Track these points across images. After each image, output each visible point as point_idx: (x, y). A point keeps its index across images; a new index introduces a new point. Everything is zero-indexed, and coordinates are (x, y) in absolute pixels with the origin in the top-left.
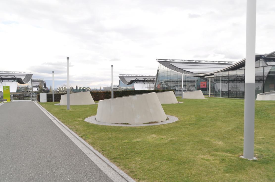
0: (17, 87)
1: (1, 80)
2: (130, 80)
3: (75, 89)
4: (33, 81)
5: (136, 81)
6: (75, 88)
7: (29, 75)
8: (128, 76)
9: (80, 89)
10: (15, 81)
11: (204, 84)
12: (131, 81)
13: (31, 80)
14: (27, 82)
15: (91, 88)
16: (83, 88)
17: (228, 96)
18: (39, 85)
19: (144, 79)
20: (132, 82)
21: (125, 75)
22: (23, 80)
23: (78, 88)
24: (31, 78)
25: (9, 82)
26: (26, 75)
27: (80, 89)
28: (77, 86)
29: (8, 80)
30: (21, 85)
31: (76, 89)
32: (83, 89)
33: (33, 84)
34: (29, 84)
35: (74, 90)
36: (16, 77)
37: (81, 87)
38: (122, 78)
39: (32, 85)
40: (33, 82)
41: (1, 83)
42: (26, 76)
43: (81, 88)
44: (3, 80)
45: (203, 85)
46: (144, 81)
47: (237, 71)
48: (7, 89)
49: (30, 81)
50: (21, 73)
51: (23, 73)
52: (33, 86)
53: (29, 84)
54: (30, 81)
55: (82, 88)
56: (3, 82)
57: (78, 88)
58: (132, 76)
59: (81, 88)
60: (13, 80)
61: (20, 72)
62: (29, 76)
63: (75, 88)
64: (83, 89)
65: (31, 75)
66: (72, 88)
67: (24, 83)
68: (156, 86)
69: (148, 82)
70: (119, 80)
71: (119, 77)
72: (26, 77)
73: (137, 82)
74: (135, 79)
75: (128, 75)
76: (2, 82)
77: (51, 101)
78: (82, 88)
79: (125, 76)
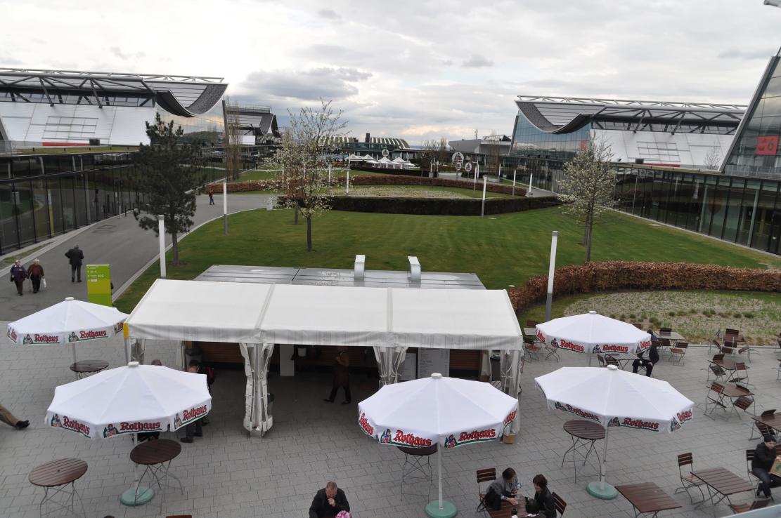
1: (100, 98)
2: (576, 115)
3: (362, 143)
6: (362, 139)
8: (548, 101)
9: (377, 142)
10: (150, 102)
12: (580, 116)
13: (219, 102)
15: (410, 143)
16: (387, 140)
17: (11, 100)
19: (632, 114)
20: (580, 123)
21: (537, 97)
23: (373, 141)
24: (221, 95)
26: (205, 87)
27: (377, 142)
28: (368, 135)
29: (124, 99)
30: (167, 117)
31: (365, 144)
32: (386, 142)
35: (360, 147)
36: (151, 88)
37: (380, 137)
38: (529, 109)
40: (227, 115)
42: (205, 90)
43: (379, 140)
47: (472, 138)
50: (190, 81)
51: (198, 81)
55: (383, 140)
56: (108, 104)
57: (373, 141)
58: (565, 101)
59: (379, 140)
60: (141, 100)
61: (189, 78)
62: (213, 91)
63: (362, 139)
64: (386, 142)
65: (223, 87)
66: (355, 139)
68: (144, 100)
69: (648, 126)
70: (517, 117)
71: (519, 104)
73: (603, 124)
74: (595, 112)
75: (548, 98)
78: (383, 140)
79: (540, 100)
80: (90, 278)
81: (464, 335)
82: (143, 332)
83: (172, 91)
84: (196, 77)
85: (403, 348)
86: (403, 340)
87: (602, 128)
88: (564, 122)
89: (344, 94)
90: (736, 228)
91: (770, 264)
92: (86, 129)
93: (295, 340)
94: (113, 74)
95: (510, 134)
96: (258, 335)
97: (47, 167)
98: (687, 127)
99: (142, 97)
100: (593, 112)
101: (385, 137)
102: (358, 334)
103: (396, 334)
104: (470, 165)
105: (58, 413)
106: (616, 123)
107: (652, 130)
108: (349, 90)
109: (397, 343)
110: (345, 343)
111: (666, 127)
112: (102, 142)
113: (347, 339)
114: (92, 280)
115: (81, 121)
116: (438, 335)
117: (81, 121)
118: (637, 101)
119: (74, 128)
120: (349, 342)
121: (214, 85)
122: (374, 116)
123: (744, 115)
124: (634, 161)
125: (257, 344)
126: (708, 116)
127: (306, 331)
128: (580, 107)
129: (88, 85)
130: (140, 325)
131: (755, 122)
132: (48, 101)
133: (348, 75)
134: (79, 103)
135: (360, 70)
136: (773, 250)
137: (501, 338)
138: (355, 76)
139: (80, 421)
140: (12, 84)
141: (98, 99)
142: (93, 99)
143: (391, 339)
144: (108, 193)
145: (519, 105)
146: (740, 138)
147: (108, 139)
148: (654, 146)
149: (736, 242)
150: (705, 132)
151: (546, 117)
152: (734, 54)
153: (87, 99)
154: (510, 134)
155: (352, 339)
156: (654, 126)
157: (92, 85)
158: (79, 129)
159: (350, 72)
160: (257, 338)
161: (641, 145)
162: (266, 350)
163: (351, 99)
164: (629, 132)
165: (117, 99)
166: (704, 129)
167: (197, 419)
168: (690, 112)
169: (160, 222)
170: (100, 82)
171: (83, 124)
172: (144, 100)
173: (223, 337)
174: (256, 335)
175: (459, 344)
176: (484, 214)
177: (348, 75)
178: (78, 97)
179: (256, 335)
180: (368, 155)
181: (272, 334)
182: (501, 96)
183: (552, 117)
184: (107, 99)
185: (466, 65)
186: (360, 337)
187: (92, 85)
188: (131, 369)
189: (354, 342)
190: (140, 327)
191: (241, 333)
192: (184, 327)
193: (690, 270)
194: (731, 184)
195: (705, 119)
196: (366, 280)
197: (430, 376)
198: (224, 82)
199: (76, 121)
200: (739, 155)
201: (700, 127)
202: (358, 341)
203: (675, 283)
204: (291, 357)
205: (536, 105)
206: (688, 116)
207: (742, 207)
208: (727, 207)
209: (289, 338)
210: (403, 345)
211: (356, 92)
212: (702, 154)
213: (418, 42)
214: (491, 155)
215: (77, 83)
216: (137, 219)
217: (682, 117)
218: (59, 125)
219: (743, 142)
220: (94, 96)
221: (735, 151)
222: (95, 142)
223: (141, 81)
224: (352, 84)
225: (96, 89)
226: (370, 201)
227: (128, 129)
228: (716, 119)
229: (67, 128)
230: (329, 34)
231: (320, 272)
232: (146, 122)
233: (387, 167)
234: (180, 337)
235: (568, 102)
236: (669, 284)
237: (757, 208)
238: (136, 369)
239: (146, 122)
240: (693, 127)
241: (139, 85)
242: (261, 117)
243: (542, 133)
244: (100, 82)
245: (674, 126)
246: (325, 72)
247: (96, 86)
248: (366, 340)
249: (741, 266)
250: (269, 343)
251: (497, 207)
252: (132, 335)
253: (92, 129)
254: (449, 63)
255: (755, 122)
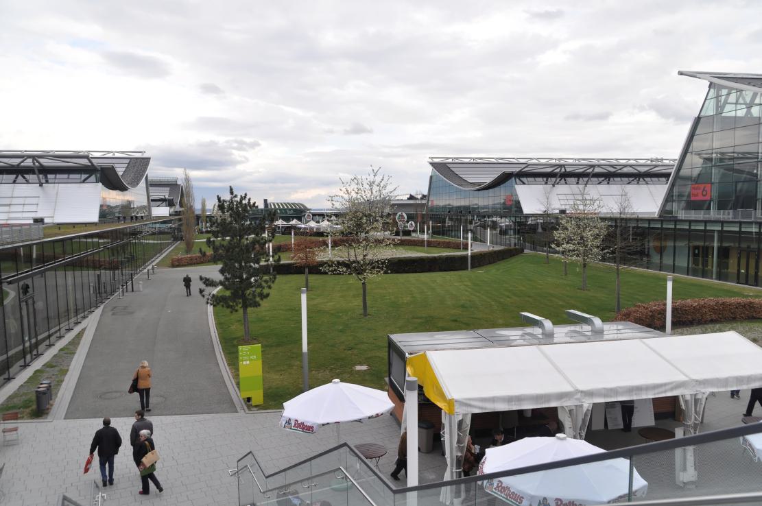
0: (101, 206)
1: (41, 176)
4: (152, 184)
5: (526, 174)
7: (139, 161)
8: (457, 161)
10: (93, 178)
11: (704, 190)
14: (135, 183)
18: (167, 197)
22: (120, 174)
25: (70, 181)
26: (128, 161)
30: (115, 198)
33: (151, 194)
34: (136, 196)
39: (148, 196)
40: (150, 188)
41: (41, 185)
44: (50, 176)
45: (701, 191)
46: (547, 176)
48: (251, 357)
49: (142, 184)
50: (110, 155)
51: (117, 155)
52: (153, 200)
53: (136, 196)
54: (142, 184)
56: (47, 182)
58: (472, 161)
60: (84, 176)
61: (109, 152)
62: (139, 164)
67: (122, 188)
68: (88, 175)
69: (563, 180)
70: (431, 177)
71: (432, 164)
72: (127, 167)
73: (524, 180)
74: (518, 170)
76: (44, 181)
77: (464, 269)
79: (450, 161)
80: (243, 361)
81: (752, 375)
82: (470, 406)
83: (116, 166)
84: (116, 152)
85: (704, 393)
86: (702, 386)
87: (524, 183)
88: (488, 180)
89: (233, 163)
90: (686, 265)
91: (751, 293)
92: (27, 208)
93: (611, 397)
94: (25, 151)
95: (426, 193)
96: (578, 396)
97: (35, 246)
98: (596, 179)
99: (84, 174)
100: (516, 169)
101: (275, 202)
102: (665, 385)
103: (697, 381)
104: (413, 223)
105: (546, 496)
106: (623, 179)
107: (566, 183)
108: (239, 159)
109: (699, 389)
110: (655, 394)
111: (578, 180)
112: (46, 221)
113: (656, 391)
114: (244, 363)
115: (21, 201)
116: (730, 377)
117: (21, 201)
118: (633, 160)
119: (13, 208)
120: (658, 393)
121: (137, 158)
122: (265, 182)
123: (675, 167)
124: (558, 211)
125: (576, 406)
126: (643, 169)
127: (620, 387)
128: (487, 166)
129: (29, 162)
130: (470, 399)
131: (683, 172)
132: (38, 181)
133: (235, 145)
134: (14, 182)
135: (248, 140)
136: (744, 282)
137: (671, 383)
138: (242, 146)
139: (577, 500)
140: (645, 172)
141: (38, 177)
142: (30, 177)
143: (694, 386)
144: (98, 272)
145: (433, 166)
146: (673, 186)
147: (52, 217)
148: (571, 197)
149: (688, 275)
150: (610, 183)
151: (457, 173)
152: (576, 117)
153: (24, 178)
154: (426, 193)
155: (660, 390)
156: (569, 180)
157: (34, 163)
158: (20, 208)
159: (236, 141)
160: (576, 399)
161: (561, 197)
162: (460, 423)
163: (240, 168)
164: (547, 186)
165: (58, 176)
166: (609, 180)
167: (506, 501)
168: (599, 166)
169: (668, 282)
170: (42, 161)
171: (14, 199)
172: (88, 175)
173: (545, 402)
174: (576, 397)
175: (747, 384)
176: (472, 267)
177: (235, 145)
178: (15, 176)
179: (576, 397)
180: (295, 220)
181: (590, 394)
182: (381, 158)
183: (468, 176)
184: (46, 177)
185: (347, 132)
186: (667, 387)
187: (34, 163)
188: (559, 441)
189: (662, 392)
190: (464, 401)
191: (561, 396)
192: (509, 396)
193: (723, 304)
194: (690, 227)
195: (609, 171)
196: (555, 336)
197: (554, 436)
198: (145, 155)
199: (15, 201)
200: (673, 201)
201: (606, 179)
202: (665, 391)
203: (713, 316)
204: (635, 410)
205: (449, 166)
206: (597, 170)
207: (689, 247)
208: (675, 247)
209: (605, 396)
210: (703, 391)
211: (247, 160)
212: (647, 202)
213: (300, 113)
214: (417, 210)
215: (16, 161)
216: (203, 296)
217: (593, 170)
218: (9, 205)
219: (676, 191)
220: (35, 174)
221: (669, 198)
222: (39, 221)
223: (87, 157)
224: (242, 153)
225: (37, 167)
226: (434, 260)
227: (80, 205)
228: (22, 164)
229: (6, 209)
230: (213, 107)
231: (498, 332)
232: (218, 196)
233: (315, 230)
234: (651, 395)
235: (475, 162)
236: (708, 318)
237: (719, 248)
238: (564, 442)
239: (218, 196)
240: (601, 179)
241: (85, 162)
242: (168, 189)
243: (461, 191)
244: (42, 161)
245: (586, 179)
246: (213, 143)
247: (37, 164)
248: (672, 389)
249: (731, 297)
250: (587, 404)
251: (476, 261)
252: (458, 411)
253: (33, 208)
254: (331, 132)
255: (683, 172)
